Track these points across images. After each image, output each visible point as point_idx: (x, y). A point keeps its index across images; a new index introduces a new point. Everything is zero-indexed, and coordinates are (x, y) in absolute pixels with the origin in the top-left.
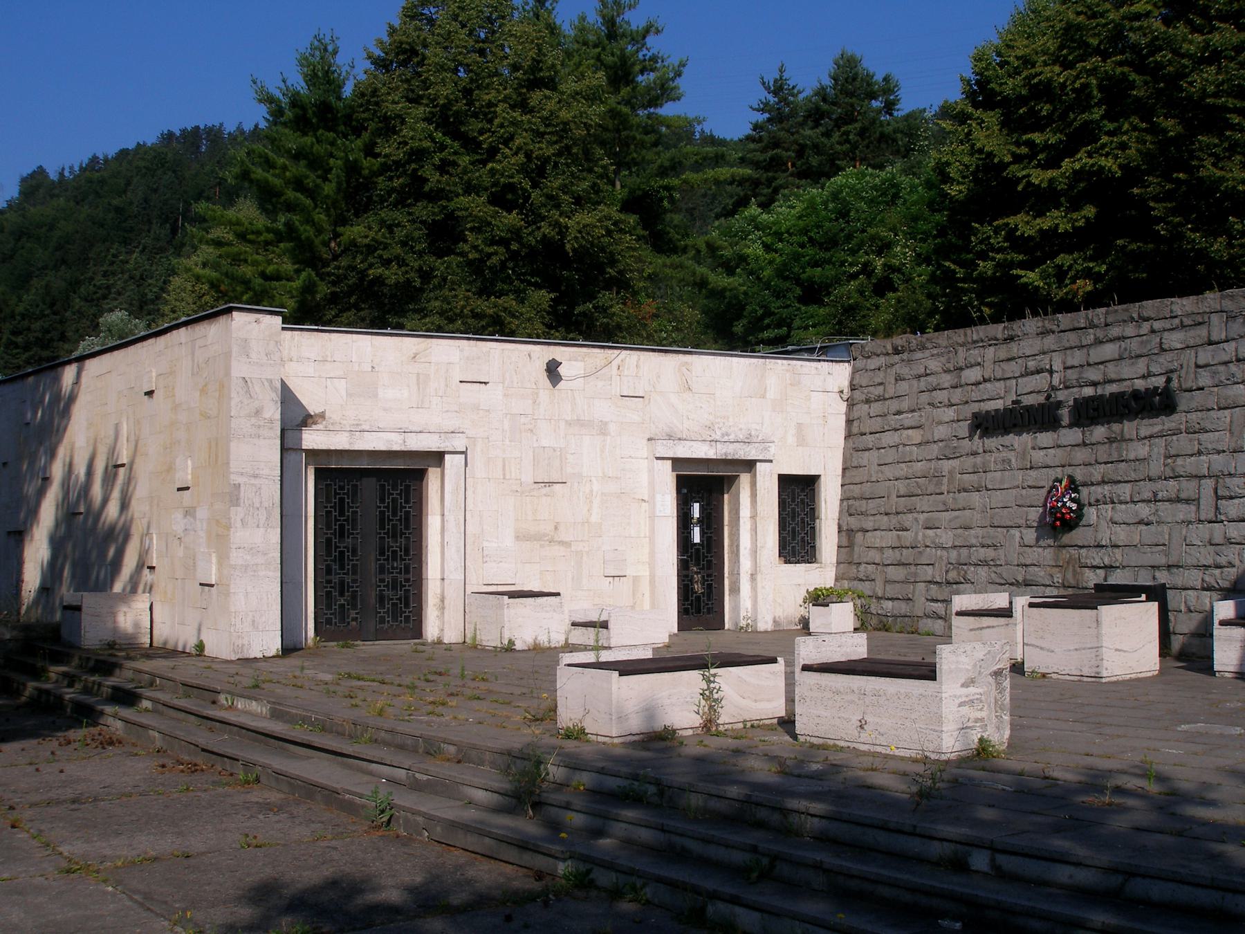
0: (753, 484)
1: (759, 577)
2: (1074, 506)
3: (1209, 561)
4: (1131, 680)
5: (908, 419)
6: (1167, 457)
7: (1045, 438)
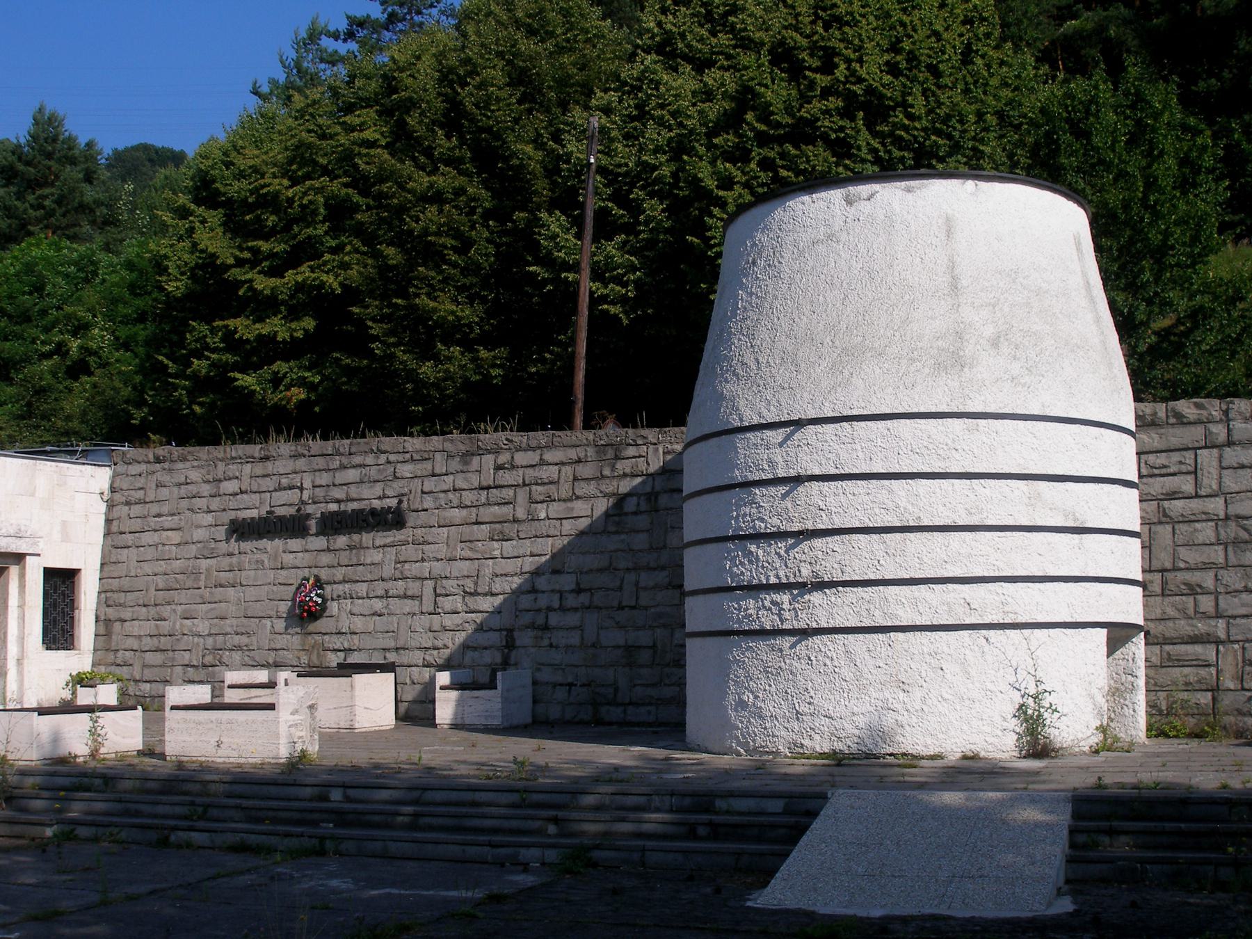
0: (22, 576)
1: (25, 661)
2: (319, 601)
3: (429, 644)
4: (375, 731)
5: (168, 521)
6: (396, 563)
7: (295, 544)
